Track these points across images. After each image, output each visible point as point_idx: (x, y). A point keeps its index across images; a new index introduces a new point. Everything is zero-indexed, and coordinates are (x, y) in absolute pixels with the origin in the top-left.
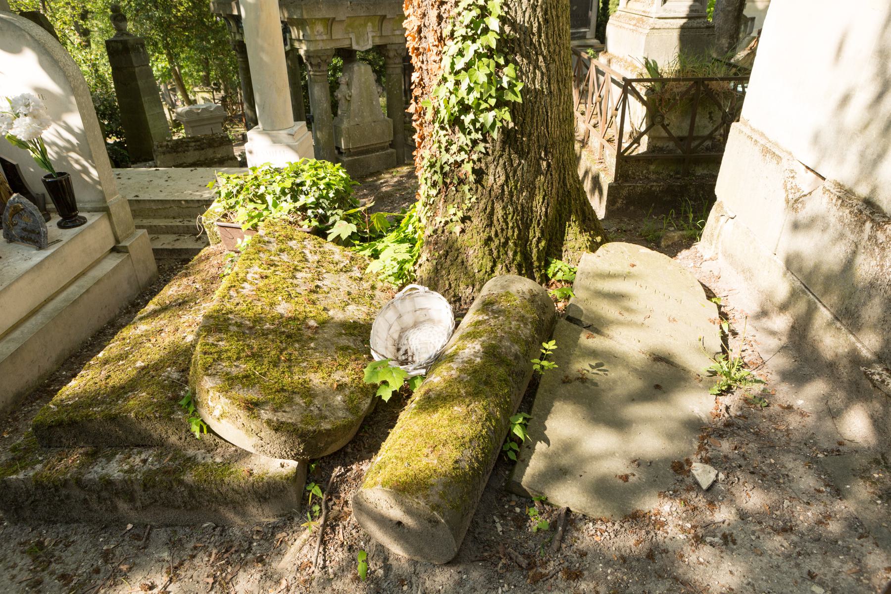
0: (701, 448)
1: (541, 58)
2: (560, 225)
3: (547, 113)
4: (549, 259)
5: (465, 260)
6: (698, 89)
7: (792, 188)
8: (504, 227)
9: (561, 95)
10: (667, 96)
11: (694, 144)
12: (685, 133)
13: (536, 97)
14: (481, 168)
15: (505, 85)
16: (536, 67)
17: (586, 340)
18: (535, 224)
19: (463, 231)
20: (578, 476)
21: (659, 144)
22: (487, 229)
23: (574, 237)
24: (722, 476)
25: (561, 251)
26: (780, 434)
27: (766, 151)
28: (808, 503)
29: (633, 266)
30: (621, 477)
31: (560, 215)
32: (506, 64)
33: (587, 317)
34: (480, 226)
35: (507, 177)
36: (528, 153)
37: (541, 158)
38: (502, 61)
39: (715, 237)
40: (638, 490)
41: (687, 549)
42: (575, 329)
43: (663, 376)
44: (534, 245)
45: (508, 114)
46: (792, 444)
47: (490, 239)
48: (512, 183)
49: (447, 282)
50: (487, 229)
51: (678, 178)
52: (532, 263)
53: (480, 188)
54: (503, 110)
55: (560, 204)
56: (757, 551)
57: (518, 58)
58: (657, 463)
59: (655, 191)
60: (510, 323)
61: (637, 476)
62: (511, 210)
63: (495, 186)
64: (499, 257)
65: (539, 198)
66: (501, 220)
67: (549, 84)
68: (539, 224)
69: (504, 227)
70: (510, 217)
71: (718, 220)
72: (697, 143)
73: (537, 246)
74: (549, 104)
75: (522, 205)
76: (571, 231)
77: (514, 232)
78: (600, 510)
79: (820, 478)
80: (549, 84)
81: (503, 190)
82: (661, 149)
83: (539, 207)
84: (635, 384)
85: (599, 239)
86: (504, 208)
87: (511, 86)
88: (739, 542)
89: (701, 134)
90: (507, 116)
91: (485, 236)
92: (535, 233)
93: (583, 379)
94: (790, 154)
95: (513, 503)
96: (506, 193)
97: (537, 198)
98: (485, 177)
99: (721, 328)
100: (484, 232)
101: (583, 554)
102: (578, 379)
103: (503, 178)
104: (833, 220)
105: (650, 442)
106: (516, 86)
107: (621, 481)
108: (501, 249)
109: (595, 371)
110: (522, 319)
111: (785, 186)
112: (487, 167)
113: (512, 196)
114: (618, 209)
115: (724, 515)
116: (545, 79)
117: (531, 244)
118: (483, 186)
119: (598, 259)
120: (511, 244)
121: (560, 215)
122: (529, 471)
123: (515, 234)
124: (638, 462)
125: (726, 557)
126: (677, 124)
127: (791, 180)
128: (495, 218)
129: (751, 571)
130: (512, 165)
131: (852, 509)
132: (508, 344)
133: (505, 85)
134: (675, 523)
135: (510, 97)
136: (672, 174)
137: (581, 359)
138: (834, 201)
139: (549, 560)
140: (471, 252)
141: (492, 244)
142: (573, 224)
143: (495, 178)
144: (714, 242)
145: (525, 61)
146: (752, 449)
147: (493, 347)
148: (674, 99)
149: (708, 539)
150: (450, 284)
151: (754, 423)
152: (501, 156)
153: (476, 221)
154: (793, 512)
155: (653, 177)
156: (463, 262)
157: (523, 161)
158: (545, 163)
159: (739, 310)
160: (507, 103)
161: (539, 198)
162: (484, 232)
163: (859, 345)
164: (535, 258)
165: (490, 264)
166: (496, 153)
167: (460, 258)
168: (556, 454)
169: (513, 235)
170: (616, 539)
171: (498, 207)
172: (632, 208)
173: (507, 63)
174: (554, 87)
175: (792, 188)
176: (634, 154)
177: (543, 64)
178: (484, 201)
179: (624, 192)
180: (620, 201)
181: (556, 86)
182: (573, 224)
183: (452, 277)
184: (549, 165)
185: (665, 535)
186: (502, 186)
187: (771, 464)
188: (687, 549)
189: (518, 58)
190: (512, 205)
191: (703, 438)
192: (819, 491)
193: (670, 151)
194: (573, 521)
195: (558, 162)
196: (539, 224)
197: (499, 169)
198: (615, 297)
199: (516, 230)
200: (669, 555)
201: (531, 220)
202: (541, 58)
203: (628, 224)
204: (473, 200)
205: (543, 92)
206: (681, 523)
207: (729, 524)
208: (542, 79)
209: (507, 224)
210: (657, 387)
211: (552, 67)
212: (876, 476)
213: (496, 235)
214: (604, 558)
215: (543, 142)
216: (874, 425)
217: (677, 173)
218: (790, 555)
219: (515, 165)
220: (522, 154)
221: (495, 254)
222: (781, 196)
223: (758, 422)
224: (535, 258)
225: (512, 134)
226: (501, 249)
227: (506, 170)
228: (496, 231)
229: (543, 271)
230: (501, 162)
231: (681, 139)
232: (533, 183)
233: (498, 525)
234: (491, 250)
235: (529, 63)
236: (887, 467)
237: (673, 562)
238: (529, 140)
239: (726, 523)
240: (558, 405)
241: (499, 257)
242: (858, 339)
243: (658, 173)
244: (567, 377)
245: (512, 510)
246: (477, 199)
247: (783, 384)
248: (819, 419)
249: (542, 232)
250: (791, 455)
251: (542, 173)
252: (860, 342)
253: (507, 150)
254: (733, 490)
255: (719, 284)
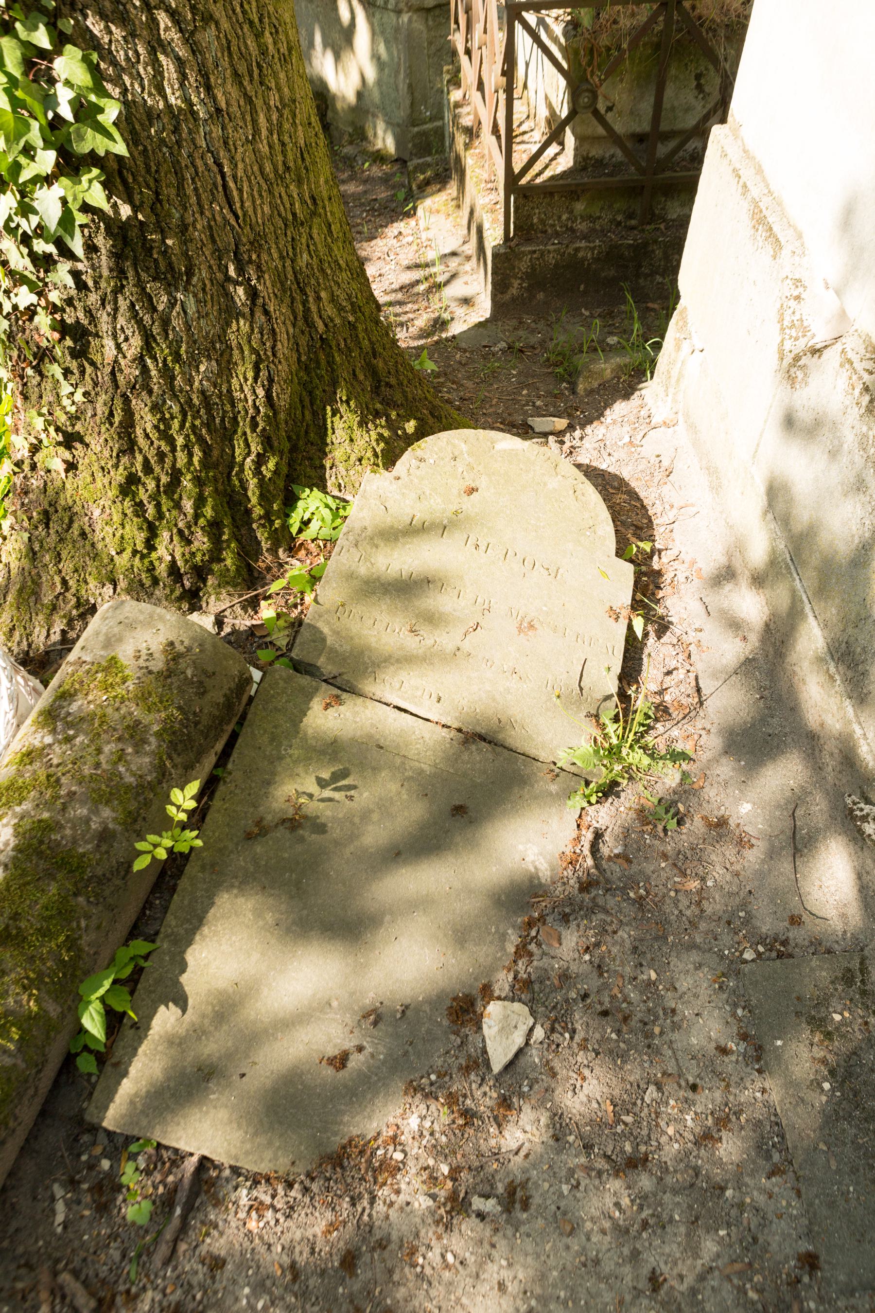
0: (522, 951)
1: (163, 19)
2: (314, 414)
3: (220, 166)
4: (295, 488)
5: (87, 529)
6: (668, 22)
7: (793, 326)
8: (165, 448)
9: (254, 112)
10: (604, 40)
11: (663, 150)
12: (645, 126)
13: (176, 130)
14: (77, 321)
15: (66, 112)
16: (156, 45)
17: (325, 718)
18: (244, 425)
19: (71, 467)
20: (236, 1078)
21: (596, 152)
22: (125, 460)
23: (348, 437)
24: (539, 1033)
25: (323, 467)
26: (684, 902)
27: (759, 220)
28: (694, 1088)
29: (472, 491)
30: (331, 1061)
31: (310, 393)
32: (58, 51)
33: (334, 655)
34: (107, 453)
35: (148, 339)
36: (190, 273)
37: (228, 279)
38: (42, 38)
39: (673, 381)
40: (362, 1090)
41: (428, 1234)
42: (302, 689)
43: (485, 771)
44: (248, 473)
45: (97, 187)
46: (703, 926)
47: (131, 482)
48: (162, 349)
49: (57, 579)
50: (125, 460)
51: (633, 228)
52: (248, 512)
53: (89, 369)
54: (85, 178)
55: (307, 369)
56: (566, 1224)
57: (95, 25)
58: (418, 1010)
59: (584, 259)
60: (99, 751)
61: (369, 1049)
62: (176, 409)
63: (122, 362)
64: (160, 516)
65: (244, 370)
66: (154, 435)
67: (209, 88)
68: (254, 425)
69: (165, 448)
70: (176, 424)
71: (678, 348)
72: (672, 144)
73: (257, 472)
74: (218, 144)
75: (203, 392)
76: (339, 424)
77: (190, 455)
78: (268, 1154)
79: (734, 1015)
80: (209, 88)
81: (145, 370)
82: (599, 163)
83: (247, 390)
84: (409, 813)
85: (411, 426)
86: (156, 408)
87: (85, 112)
88: (536, 1200)
89: (679, 126)
90: (97, 196)
91: (119, 476)
92: (247, 449)
93: (296, 823)
94: (800, 236)
95: (98, 1150)
96: (154, 373)
97: (241, 369)
98: (94, 342)
99: (630, 627)
100: (116, 466)
101: (216, 1264)
102: (284, 821)
103: (136, 342)
104: (849, 438)
105: (411, 962)
106: (101, 110)
107: (330, 1071)
108: (164, 499)
109: (327, 793)
110: (134, 733)
111: (781, 320)
112: (93, 319)
113: (173, 378)
114: (514, 299)
115: (521, 1134)
116: (192, 77)
117: (242, 470)
118: (93, 364)
119: (396, 485)
120: (187, 482)
121: (310, 393)
122: (127, 1088)
123: (196, 460)
124: (375, 1016)
125: (502, 1244)
126: (625, 104)
127: (793, 303)
128: (139, 431)
129: (542, 1277)
130: (155, 309)
131: (775, 1097)
132: (82, 811)
133: (66, 112)
134: (422, 1162)
135: (91, 142)
136: (619, 218)
137: (300, 770)
138: (857, 392)
139: (144, 1289)
140: (97, 513)
141: (141, 491)
142: (343, 408)
143: (117, 344)
144: (671, 390)
145: (118, 33)
146: (622, 944)
147: (45, 827)
148: (619, 48)
149: (477, 1203)
150: (64, 582)
151: (641, 872)
152: (118, 290)
153: (96, 443)
154: (658, 1114)
155: (582, 226)
156: (83, 534)
157: (179, 296)
158: (240, 291)
159: (688, 559)
160: (93, 159)
161: (244, 370)
162: (116, 466)
163: (858, 732)
164: (254, 500)
165: (140, 538)
166: (103, 284)
167: (76, 525)
168: (198, 1033)
169: (190, 462)
170: (289, 1223)
171: (141, 407)
172: (541, 296)
173: (60, 40)
174: (226, 93)
175: (793, 326)
176: (539, 181)
177: (174, 35)
178: (103, 398)
179: (523, 265)
180: (516, 283)
181: (234, 92)
182: (343, 408)
183: (67, 566)
184: (253, 294)
185: (393, 1197)
186: (140, 360)
187: (649, 983)
188: (428, 1234)
189: (95, 25)
190: (175, 396)
191: (530, 925)
192: (723, 1051)
193: (618, 168)
194: (213, 1183)
195: (280, 279)
196: (254, 425)
197: (121, 321)
198: (405, 590)
199: (197, 450)
200: (386, 1254)
201: (235, 419)
202: (163, 19)
203: (533, 331)
204: (79, 397)
205: (194, 113)
206: (431, 1162)
207: (527, 1156)
208: (183, 77)
209: (171, 442)
210: (459, 810)
211: (208, 36)
212: (837, 1017)
213: (148, 468)
214: (256, 1273)
215: (226, 239)
216: (860, 891)
217: (630, 216)
218: (627, 1231)
219: (161, 308)
220: (171, 279)
221: (151, 511)
222: (769, 340)
223: (649, 868)
224: (254, 500)
225: (133, 233)
226: (164, 499)
227: (140, 322)
228: (146, 461)
229: (277, 523)
230: (123, 304)
231: (640, 138)
232: (222, 337)
233: (60, 1207)
234: (141, 504)
235: (132, 35)
236: (864, 993)
237: (390, 1272)
238: (185, 241)
239: (522, 1153)
240: (224, 901)
241: (160, 516)
242: (857, 716)
243: (591, 218)
244: (259, 823)
245: (92, 1166)
246: (86, 394)
247: (724, 760)
248: (772, 854)
249: (267, 441)
250: (695, 956)
251: (240, 314)
252: (860, 723)
253: (131, 274)
254: (557, 1064)
255: (666, 490)
